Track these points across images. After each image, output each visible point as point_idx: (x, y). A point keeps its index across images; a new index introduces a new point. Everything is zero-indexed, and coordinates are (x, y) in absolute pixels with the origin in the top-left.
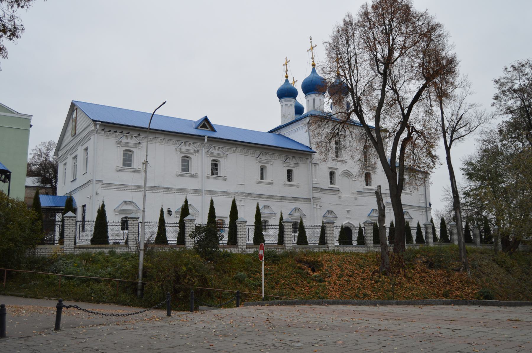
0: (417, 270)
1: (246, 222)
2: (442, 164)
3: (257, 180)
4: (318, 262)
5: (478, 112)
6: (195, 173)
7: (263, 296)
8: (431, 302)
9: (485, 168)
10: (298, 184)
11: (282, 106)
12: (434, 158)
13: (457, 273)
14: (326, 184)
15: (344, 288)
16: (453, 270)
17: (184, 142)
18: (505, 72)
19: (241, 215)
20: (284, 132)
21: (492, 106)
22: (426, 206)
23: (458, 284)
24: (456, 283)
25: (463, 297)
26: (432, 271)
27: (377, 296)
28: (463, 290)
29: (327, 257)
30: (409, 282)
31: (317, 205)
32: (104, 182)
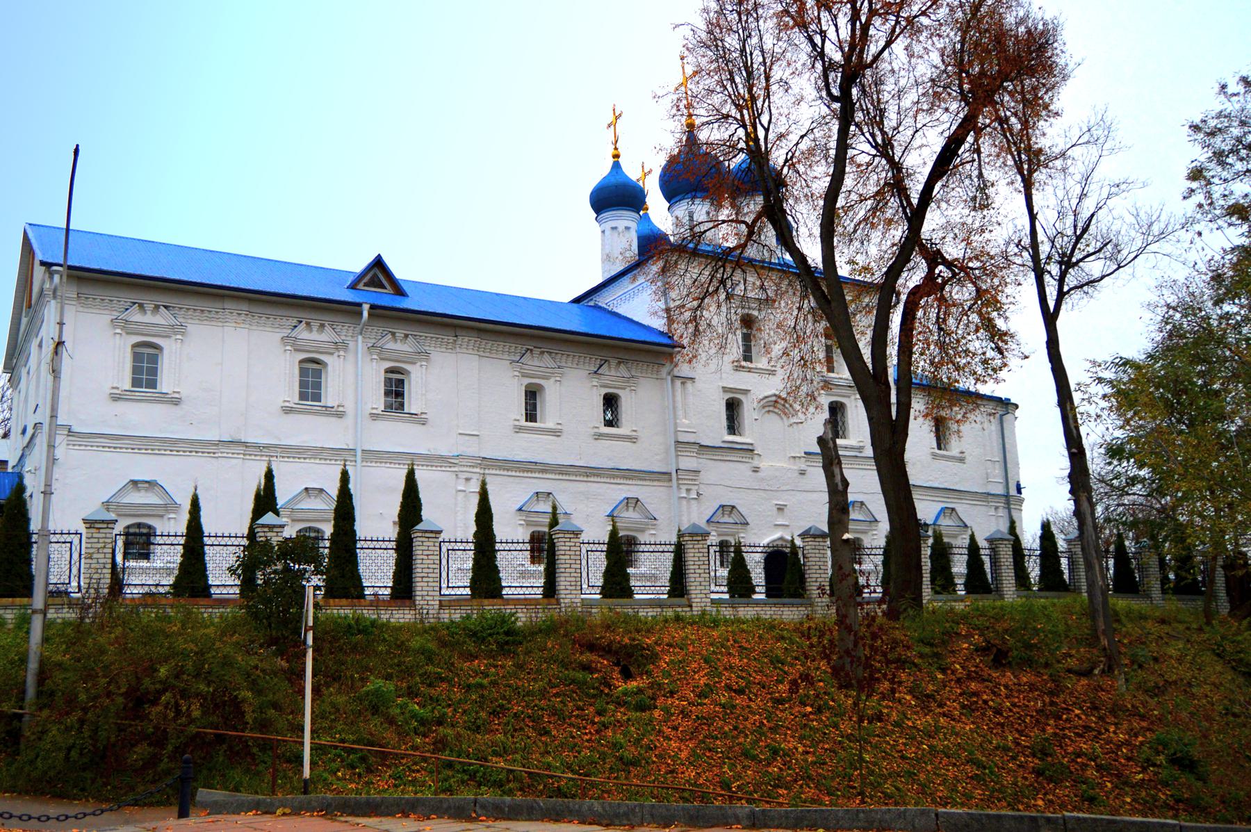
0: (954, 672)
1: (440, 532)
2: (1026, 357)
3: (517, 423)
4: (644, 649)
5: (1142, 214)
6: (335, 404)
7: (307, 773)
8: (887, 817)
9: (1178, 385)
10: (634, 433)
11: (603, 232)
12: (999, 338)
13: (1084, 681)
14: (716, 433)
15: (712, 728)
16: (1069, 671)
17: (304, 321)
18: (1222, 96)
19: (430, 514)
20: (604, 300)
21: (1184, 198)
22: (1008, 492)
23: (1083, 717)
24: (1077, 712)
25: (1097, 757)
26: (1004, 676)
27: (814, 753)
28: (1100, 733)
29: (678, 634)
30: (926, 710)
31: (688, 490)
32: (75, 429)
